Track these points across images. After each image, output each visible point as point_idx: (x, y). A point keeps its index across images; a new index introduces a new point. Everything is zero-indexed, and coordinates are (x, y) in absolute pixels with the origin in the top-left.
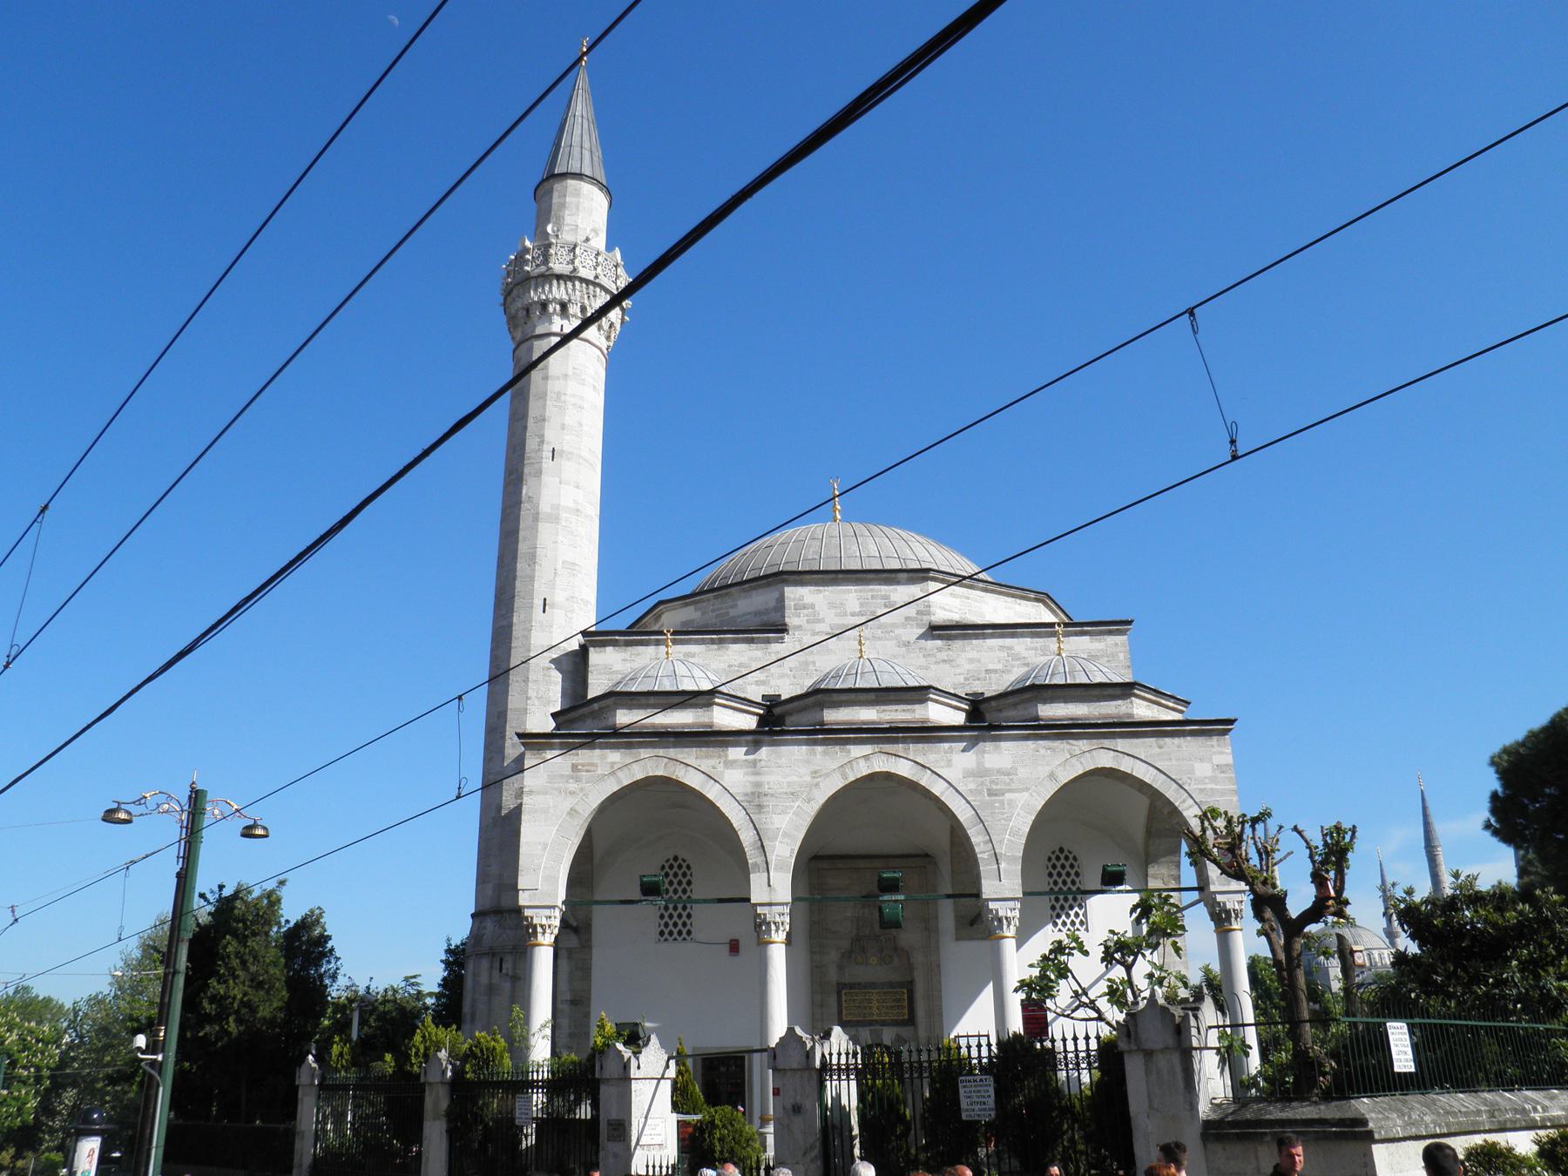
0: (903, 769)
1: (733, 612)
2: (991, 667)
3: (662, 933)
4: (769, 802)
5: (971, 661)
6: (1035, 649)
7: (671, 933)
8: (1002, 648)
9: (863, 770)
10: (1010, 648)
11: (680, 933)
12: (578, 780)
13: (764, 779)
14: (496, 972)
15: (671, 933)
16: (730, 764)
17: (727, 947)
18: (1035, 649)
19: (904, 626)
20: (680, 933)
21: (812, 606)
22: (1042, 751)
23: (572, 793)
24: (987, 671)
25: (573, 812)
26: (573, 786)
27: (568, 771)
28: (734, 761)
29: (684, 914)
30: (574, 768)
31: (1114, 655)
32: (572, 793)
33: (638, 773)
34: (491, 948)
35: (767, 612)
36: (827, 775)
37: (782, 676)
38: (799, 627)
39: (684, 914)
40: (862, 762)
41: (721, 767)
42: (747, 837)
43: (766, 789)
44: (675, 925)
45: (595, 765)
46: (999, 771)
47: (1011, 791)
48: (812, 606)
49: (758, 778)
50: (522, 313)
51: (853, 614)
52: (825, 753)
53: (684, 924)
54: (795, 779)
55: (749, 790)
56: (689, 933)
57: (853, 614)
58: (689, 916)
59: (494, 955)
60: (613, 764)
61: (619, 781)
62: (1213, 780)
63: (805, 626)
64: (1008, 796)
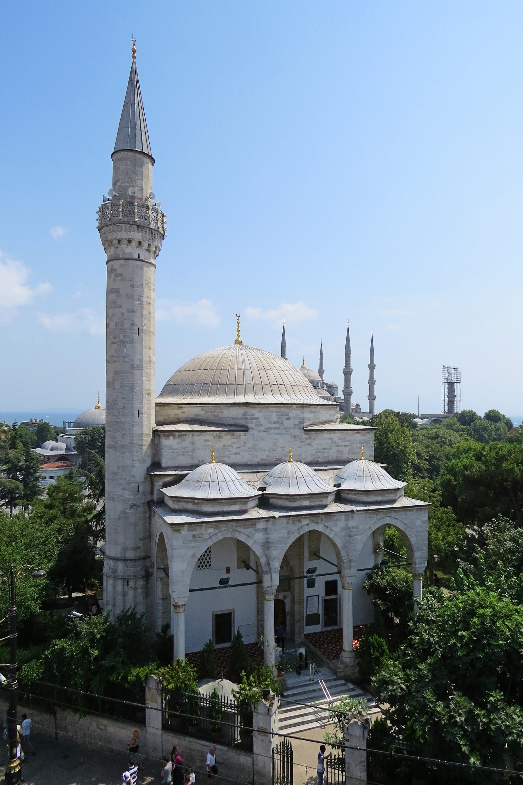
0: (320, 528)
1: (221, 415)
2: (325, 447)
3: (199, 567)
4: (272, 545)
5: (318, 444)
6: (341, 439)
7: (202, 566)
8: (330, 438)
9: (306, 529)
10: (332, 439)
11: (206, 566)
12: (195, 542)
13: (271, 536)
14: (126, 587)
15: (202, 566)
16: (257, 530)
17: (225, 570)
18: (341, 439)
19: (294, 428)
20: (206, 566)
21: (258, 418)
22: (368, 518)
23: (193, 548)
24: (324, 449)
25: (193, 556)
26: (193, 544)
27: (191, 538)
28: (258, 529)
29: (208, 558)
30: (194, 536)
31: (368, 442)
32: (193, 548)
33: (220, 537)
34: (123, 576)
35: (238, 419)
36: (293, 533)
37: (245, 451)
38: (252, 428)
39: (208, 558)
40: (306, 526)
41: (253, 532)
42: (263, 561)
43: (270, 541)
44: (204, 562)
45: (202, 534)
46: (353, 527)
47: (356, 535)
48: (258, 418)
49: (267, 536)
50: (115, 242)
51: (274, 423)
52: (293, 523)
53: (208, 562)
54: (281, 535)
55: (263, 541)
56: (210, 565)
57: (274, 423)
58: (210, 558)
59: (124, 579)
60: (210, 533)
61: (212, 541)
62: (421, 527)
63: (255, 427)
64: (355, 537)
